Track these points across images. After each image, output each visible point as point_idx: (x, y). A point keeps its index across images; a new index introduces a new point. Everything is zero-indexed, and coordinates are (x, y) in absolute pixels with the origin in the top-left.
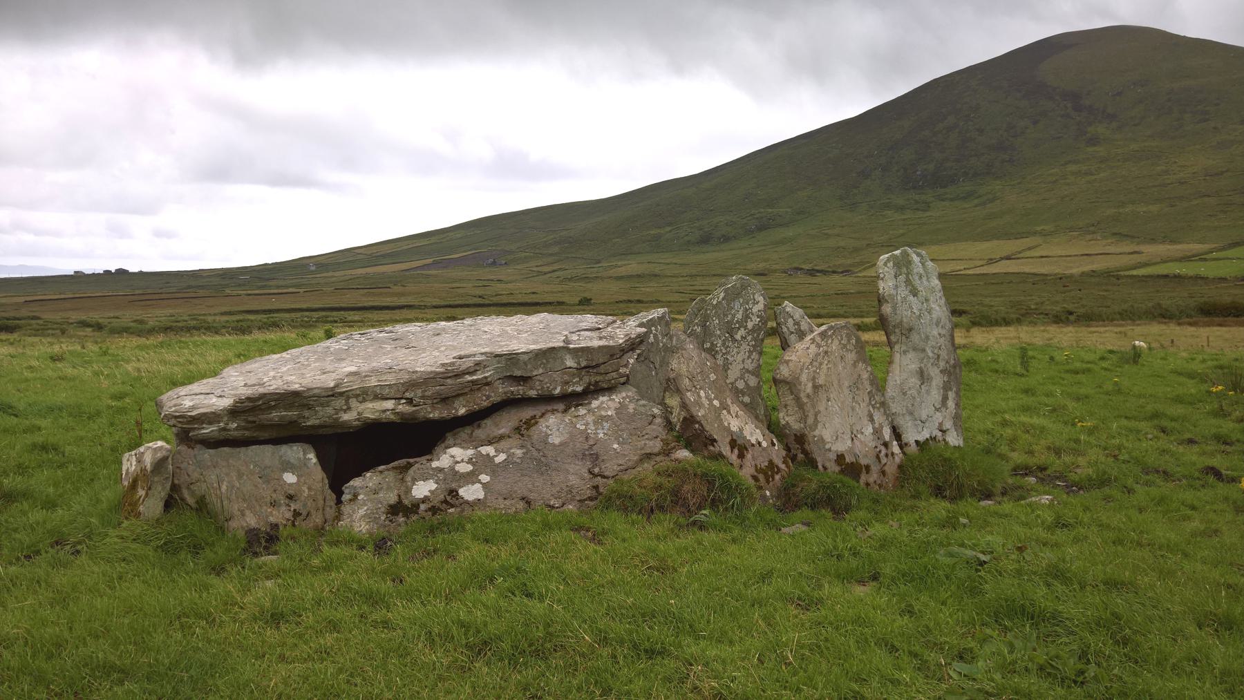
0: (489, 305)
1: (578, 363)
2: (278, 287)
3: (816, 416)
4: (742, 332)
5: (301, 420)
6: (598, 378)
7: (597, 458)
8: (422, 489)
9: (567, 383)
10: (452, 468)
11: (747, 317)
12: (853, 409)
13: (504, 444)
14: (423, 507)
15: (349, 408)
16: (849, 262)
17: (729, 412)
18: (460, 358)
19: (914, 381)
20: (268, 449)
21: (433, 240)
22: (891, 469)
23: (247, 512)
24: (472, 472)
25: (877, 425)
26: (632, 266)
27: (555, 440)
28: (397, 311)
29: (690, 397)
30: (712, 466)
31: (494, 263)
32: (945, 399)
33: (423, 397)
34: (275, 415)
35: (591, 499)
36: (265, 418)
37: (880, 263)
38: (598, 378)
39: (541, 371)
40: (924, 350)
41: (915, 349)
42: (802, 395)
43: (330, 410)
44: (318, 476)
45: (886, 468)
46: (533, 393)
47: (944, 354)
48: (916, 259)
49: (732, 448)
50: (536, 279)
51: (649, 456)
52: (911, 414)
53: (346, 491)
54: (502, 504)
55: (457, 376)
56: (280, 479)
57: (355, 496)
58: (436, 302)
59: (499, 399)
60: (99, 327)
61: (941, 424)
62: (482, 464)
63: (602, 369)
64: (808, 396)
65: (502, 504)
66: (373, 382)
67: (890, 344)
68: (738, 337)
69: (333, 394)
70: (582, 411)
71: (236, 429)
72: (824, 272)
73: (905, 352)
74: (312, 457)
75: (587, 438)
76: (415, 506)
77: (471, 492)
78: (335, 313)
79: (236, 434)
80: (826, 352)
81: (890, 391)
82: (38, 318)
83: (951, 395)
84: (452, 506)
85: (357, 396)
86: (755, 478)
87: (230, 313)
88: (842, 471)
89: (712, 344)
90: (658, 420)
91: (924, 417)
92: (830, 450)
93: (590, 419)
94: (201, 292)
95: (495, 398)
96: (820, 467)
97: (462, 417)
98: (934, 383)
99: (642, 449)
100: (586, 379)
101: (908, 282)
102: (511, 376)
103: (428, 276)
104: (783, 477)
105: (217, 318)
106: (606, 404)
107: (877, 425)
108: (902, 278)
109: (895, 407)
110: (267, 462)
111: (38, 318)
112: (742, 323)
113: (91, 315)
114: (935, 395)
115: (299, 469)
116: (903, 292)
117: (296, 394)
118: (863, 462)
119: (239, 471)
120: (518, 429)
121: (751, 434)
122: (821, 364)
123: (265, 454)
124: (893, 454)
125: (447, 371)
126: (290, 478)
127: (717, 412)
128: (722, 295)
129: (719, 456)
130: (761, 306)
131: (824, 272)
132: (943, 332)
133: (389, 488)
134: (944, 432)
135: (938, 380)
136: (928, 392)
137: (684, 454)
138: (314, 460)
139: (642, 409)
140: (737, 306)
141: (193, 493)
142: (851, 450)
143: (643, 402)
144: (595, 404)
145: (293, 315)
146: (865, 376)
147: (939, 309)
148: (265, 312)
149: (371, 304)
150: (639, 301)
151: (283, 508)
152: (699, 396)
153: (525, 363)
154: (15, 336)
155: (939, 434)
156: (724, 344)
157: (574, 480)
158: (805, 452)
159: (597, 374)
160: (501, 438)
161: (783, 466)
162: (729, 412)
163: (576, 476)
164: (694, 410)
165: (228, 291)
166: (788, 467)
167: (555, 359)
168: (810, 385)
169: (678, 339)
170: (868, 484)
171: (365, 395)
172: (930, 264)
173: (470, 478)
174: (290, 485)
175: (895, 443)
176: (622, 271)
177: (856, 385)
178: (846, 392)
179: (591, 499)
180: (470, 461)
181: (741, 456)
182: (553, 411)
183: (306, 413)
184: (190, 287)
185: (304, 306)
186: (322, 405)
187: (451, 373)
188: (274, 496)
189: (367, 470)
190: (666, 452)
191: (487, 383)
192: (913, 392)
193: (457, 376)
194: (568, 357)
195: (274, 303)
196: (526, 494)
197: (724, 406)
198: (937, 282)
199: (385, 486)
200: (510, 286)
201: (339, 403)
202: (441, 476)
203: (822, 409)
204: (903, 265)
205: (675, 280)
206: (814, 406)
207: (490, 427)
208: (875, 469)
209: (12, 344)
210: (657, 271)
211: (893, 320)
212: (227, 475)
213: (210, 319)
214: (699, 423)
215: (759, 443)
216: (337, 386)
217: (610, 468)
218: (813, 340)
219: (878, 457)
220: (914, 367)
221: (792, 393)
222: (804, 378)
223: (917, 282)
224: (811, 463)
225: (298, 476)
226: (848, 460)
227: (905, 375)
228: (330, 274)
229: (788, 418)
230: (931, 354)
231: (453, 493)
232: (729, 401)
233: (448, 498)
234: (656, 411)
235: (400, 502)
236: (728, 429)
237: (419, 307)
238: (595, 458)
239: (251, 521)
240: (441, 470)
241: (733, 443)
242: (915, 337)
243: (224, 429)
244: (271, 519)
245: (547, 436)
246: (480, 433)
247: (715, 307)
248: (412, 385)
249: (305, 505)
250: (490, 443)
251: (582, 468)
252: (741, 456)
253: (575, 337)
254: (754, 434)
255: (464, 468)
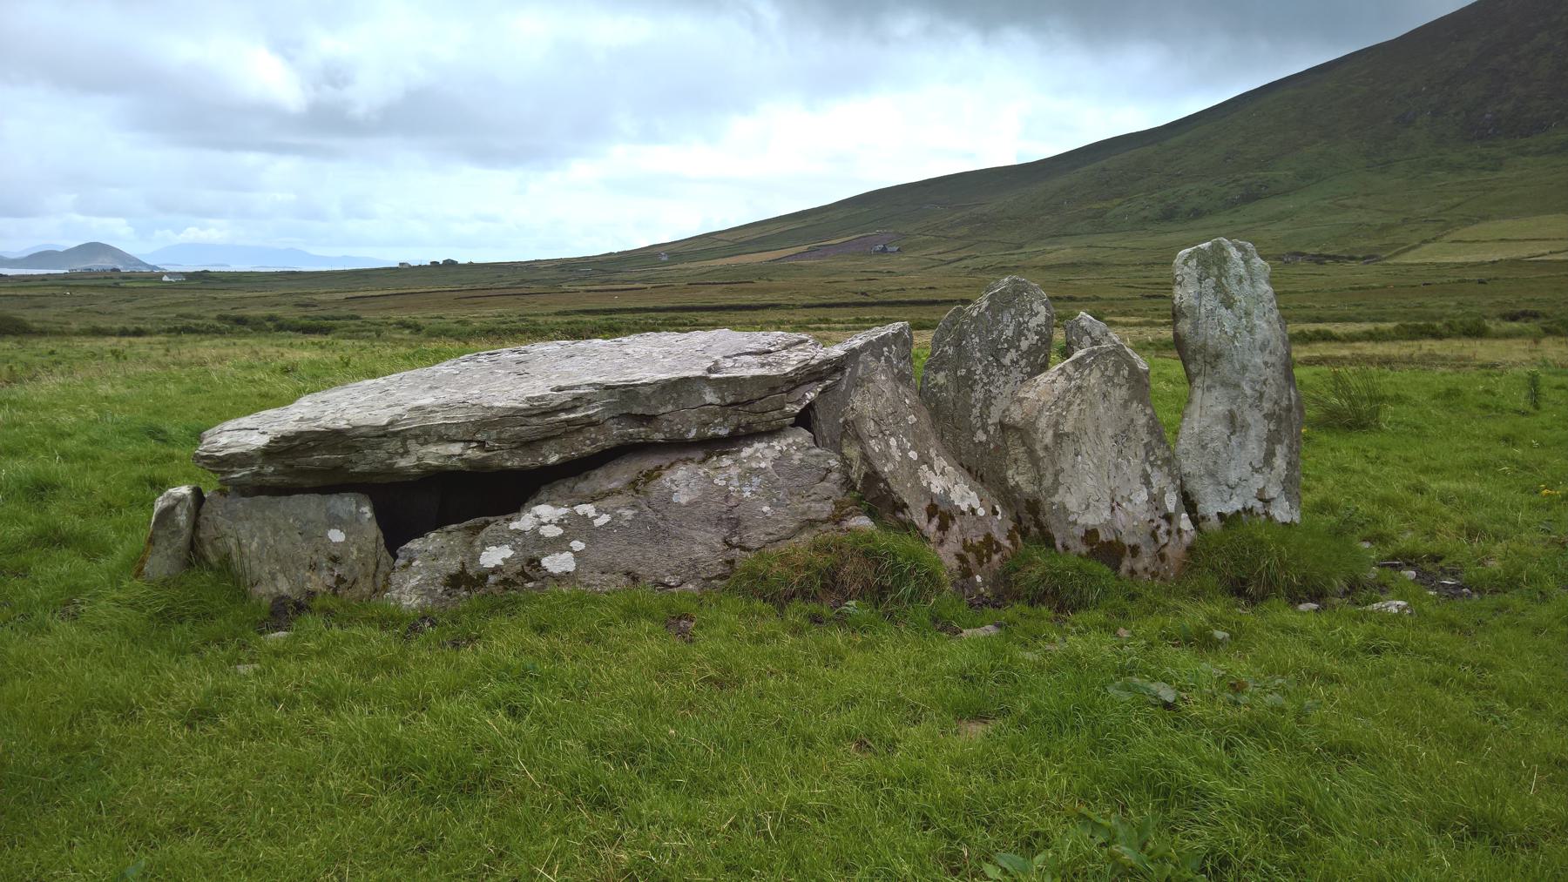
0: (873, 304)
1: (723, 398)
2: (624, 282)
3: (1056, 475)
4: (1012, 354)
5: (347, 466)
6: (751, 418)
7: (737, 524)
8: (493, 557)
9: (706, 424)
10: (535, 532)
11: (1020, 333)
12: (1117, 467)
13: (609, 503)
14: (492, 579)
15: (407, 452)
16: (1375, 243)
17: (931, 468)
18: (560, 389)
19: (1220, 429)
20: (314, 499)
21: (810, 220)
22: (1175, 551)
23: (280, 576)
24: (561, 537)
25: (1155, 491)
26: (1065, 251)
27: (682, 498)
28: (867, 309)
29: (875, 446)
30: (887, 540)
31: (884, 250)
32: (1269, 456)
33: (498, 440)
34: (317, 458)
35: (721, 577)
36: (302, 461)
37: (1178, 261)
38: (751, 418)
39: (670, 408)
40: (1237, 386)
41: (1224, 384)
42: (1038, 447)
43: (382, 454)
44: (372, 531)
45: (1167, 550)
46: (658, 437)
47: (1271, 391)
48: (1234, 254)
49: (930, 516)
50: (935, 270)
51: (812, 523)
52: (1212, 475)
53: (401, 555)
54: (597, 579)
55: (545, 414)
56: (324, 536)
57: (411, 561)
58: (808, 300)
59: (613, 443)
60: (417, 329)
61: (1262, 491)
62: (575, 527)
63: (757, 406)
64: (1046, 448)
65: (597, 579)
66: (438, 419)
67: (1190, 378)
68: (1006, 361)
69: (384, 434)
70: (726, 461)
71: (273, 474)
72: (1335, 258)
73: (1209, 388)
74: (367, 511)
75: (727, 498)
76: (483, 576)
77: (557, 563)
78: (686, 314)
79: (273, 479)
80: (1079, 388)
81: (1184, 444)
82: (358, 318)
83: (1280, 450)
84: (530, 579)
85: (416, 437)
86: (960, 557)
87: (566, 313)
88: (1092, 554)
89: (969, 371)
90: (835, 476)
91: (1233, 479)
92: (1075, 523)
93: (734, 471)
94: (535, 288)
95: (604, 442)
96: (1059, 546)
97: (554, 466)
98: (1252, 433)
99: (804, 513)
100: (734, 420)
101: (1219, 288)
102: (629, 415)
103: (800, 268)
104: (1005, 558)
105: (550, 319)
106: (760, 454)
107: (1155, 491)
108: (1211, 282)
109: (1189, 466)
110: (311, 515)
111: (358, 318)
112: (1013, 343)
113: (414, 314)
114: (1255, 450)
115: (347, 527)
116: (1210, 302)
117: (338, 433)
118: (1128, 540)
119: (275, 526)
120: (633, 484)
121: (962, 498)
122: (1070, 404)
123: (309, 506)
124: (1179, 531)
125: (532, 408)
126: (336, 536)
127: (914, 467)
128: (985, 304)
129: (908, 527)
130: (1041, 319)
131: (1335, 258)
132: (1272, 359)
133: (452, 554)
134: (1267, 502)
135: (1258, 427)
136: (1241, 445)
137: (862, 522)
138: (369, 515)
139: (813, 461)
140: (1006, 318)
141: (215, 550)
142: (1108, 525)
143: (817, 451)
144: (747, 452)
145: (637, 316)
146: (1142, 420)
147: (1266, 327)
148: (605, 312)
149: (735, 303)
150: (1071, 299)
151: (325, 573)
152: (888, 445)
153: (648, 398)
154: (329, 338)
155: (1259, 505)
156: (985, 371)
157: (700, 552)
158: (1039, 524)
159: (746, 412)
160: (610, 493)
161: (1007, 543)
162: (931, 468)
163: (705, 545)
164: (878, 465)
165: (565, 287)
166: (1014, 543)
167: (689, 393)
168: (1050, 433)
169: (866, 367)
170: (1133, 572)
171: (427, 435)
172: (1258, 262)
173: (558, 544)
174: (336, 544)
175: (1185, 515)
176: (1051, 258)
177: (1123, 436)
178: (1108, 443)
179: (721, 577)
180: (560, 523)
181: (943, 527)
182: (685, 462)
183: (353, 457)
184: (524, 281)
185: (651, 305)
186: (371, 447)
187: (540, 410)
188: (315, 557)
189: (432, 530)
190: (837, 519)
191: (589, 423)
192: (1218, 445)
193: (545, 414)
194: (708, 390)
195: (617, 301)
196: (632, 567)
197: (925, 460)
198: (1266, 287)
199: (447, 551)
200: (902, 279)
201: (394, 445)
202: (520, 540)
203: (1066, 466)
204: (1213, 263)
205: (1123, 269)
206: (1053, 463)
207: (601, 480)
208: (1147, 552)
209: (322, 347)
210: (1099, 258)
211: (1193, 342)
212: (261, 529)
213: (541, 320)
214: (885, 481)
215: (973, 511)
216: (391, 423)
217: (755, 537)
218: (1063, 370)
219: (1154, 535)
220: (1221, 409)
221: (1024, 444)
222: (1042, 423)
223: (1233, 288)
224: (1047, 540)
225: (347, 534)
226: (1102, 537)
227: (1206, 421)
228: (685, 265)
229: (1019, 477)
230: (1248, 391)
231: (534, 563)
232: (933, 453)
233: (527, 569)
234: (833, 463)
235: (463, 572)
236: (927, 491)
237: (786, 307)
238: (736, 524)
239: (284, 586)
240: (520, 533)
241: (932, 511)
242: (1224, 368)
243: (257, 474)
244: (309, 586)
245: (671, 493)
246: (584, 487)
247: (974, 320)
248: (484, 424)
249: (351, 570)
250: (592, 500)
251: (715, 537)
252: (943, 527)
253: (729, 363)
254: (965, 496)
255: (552, 532)
